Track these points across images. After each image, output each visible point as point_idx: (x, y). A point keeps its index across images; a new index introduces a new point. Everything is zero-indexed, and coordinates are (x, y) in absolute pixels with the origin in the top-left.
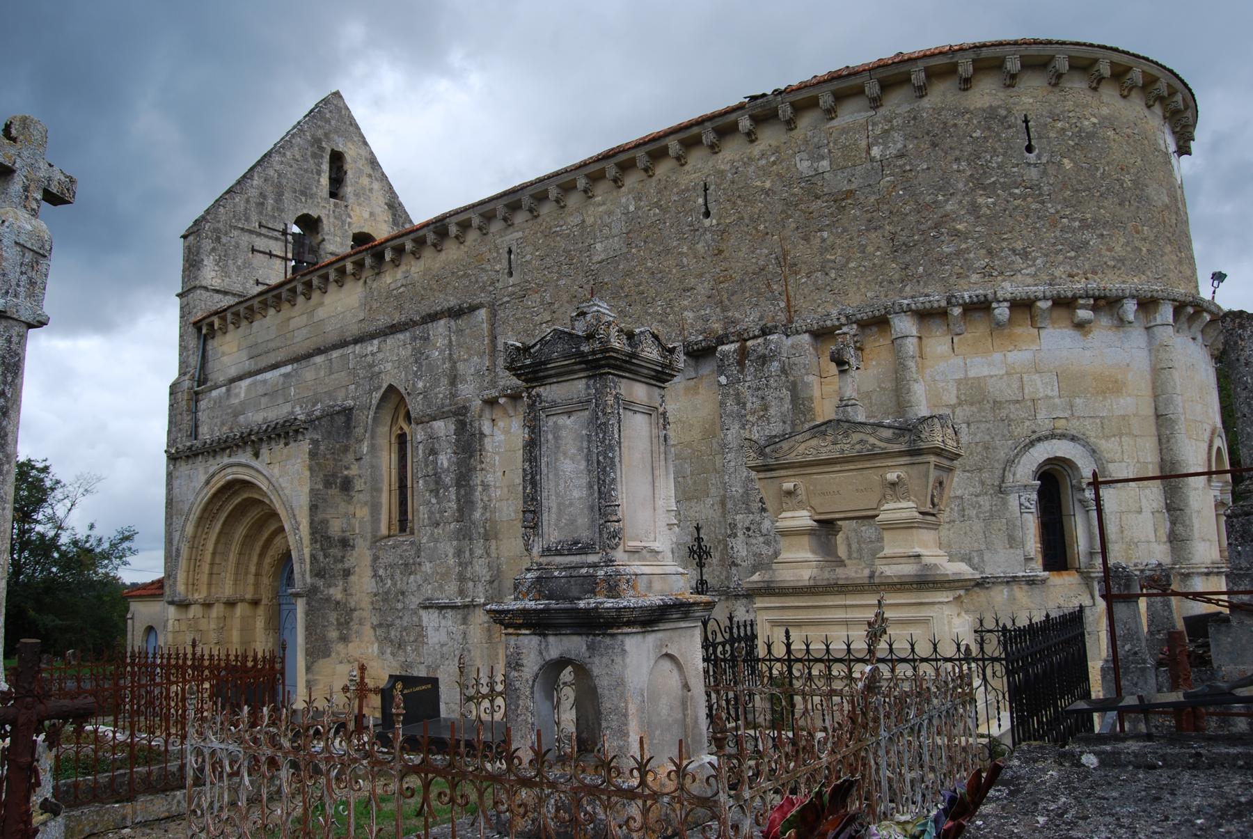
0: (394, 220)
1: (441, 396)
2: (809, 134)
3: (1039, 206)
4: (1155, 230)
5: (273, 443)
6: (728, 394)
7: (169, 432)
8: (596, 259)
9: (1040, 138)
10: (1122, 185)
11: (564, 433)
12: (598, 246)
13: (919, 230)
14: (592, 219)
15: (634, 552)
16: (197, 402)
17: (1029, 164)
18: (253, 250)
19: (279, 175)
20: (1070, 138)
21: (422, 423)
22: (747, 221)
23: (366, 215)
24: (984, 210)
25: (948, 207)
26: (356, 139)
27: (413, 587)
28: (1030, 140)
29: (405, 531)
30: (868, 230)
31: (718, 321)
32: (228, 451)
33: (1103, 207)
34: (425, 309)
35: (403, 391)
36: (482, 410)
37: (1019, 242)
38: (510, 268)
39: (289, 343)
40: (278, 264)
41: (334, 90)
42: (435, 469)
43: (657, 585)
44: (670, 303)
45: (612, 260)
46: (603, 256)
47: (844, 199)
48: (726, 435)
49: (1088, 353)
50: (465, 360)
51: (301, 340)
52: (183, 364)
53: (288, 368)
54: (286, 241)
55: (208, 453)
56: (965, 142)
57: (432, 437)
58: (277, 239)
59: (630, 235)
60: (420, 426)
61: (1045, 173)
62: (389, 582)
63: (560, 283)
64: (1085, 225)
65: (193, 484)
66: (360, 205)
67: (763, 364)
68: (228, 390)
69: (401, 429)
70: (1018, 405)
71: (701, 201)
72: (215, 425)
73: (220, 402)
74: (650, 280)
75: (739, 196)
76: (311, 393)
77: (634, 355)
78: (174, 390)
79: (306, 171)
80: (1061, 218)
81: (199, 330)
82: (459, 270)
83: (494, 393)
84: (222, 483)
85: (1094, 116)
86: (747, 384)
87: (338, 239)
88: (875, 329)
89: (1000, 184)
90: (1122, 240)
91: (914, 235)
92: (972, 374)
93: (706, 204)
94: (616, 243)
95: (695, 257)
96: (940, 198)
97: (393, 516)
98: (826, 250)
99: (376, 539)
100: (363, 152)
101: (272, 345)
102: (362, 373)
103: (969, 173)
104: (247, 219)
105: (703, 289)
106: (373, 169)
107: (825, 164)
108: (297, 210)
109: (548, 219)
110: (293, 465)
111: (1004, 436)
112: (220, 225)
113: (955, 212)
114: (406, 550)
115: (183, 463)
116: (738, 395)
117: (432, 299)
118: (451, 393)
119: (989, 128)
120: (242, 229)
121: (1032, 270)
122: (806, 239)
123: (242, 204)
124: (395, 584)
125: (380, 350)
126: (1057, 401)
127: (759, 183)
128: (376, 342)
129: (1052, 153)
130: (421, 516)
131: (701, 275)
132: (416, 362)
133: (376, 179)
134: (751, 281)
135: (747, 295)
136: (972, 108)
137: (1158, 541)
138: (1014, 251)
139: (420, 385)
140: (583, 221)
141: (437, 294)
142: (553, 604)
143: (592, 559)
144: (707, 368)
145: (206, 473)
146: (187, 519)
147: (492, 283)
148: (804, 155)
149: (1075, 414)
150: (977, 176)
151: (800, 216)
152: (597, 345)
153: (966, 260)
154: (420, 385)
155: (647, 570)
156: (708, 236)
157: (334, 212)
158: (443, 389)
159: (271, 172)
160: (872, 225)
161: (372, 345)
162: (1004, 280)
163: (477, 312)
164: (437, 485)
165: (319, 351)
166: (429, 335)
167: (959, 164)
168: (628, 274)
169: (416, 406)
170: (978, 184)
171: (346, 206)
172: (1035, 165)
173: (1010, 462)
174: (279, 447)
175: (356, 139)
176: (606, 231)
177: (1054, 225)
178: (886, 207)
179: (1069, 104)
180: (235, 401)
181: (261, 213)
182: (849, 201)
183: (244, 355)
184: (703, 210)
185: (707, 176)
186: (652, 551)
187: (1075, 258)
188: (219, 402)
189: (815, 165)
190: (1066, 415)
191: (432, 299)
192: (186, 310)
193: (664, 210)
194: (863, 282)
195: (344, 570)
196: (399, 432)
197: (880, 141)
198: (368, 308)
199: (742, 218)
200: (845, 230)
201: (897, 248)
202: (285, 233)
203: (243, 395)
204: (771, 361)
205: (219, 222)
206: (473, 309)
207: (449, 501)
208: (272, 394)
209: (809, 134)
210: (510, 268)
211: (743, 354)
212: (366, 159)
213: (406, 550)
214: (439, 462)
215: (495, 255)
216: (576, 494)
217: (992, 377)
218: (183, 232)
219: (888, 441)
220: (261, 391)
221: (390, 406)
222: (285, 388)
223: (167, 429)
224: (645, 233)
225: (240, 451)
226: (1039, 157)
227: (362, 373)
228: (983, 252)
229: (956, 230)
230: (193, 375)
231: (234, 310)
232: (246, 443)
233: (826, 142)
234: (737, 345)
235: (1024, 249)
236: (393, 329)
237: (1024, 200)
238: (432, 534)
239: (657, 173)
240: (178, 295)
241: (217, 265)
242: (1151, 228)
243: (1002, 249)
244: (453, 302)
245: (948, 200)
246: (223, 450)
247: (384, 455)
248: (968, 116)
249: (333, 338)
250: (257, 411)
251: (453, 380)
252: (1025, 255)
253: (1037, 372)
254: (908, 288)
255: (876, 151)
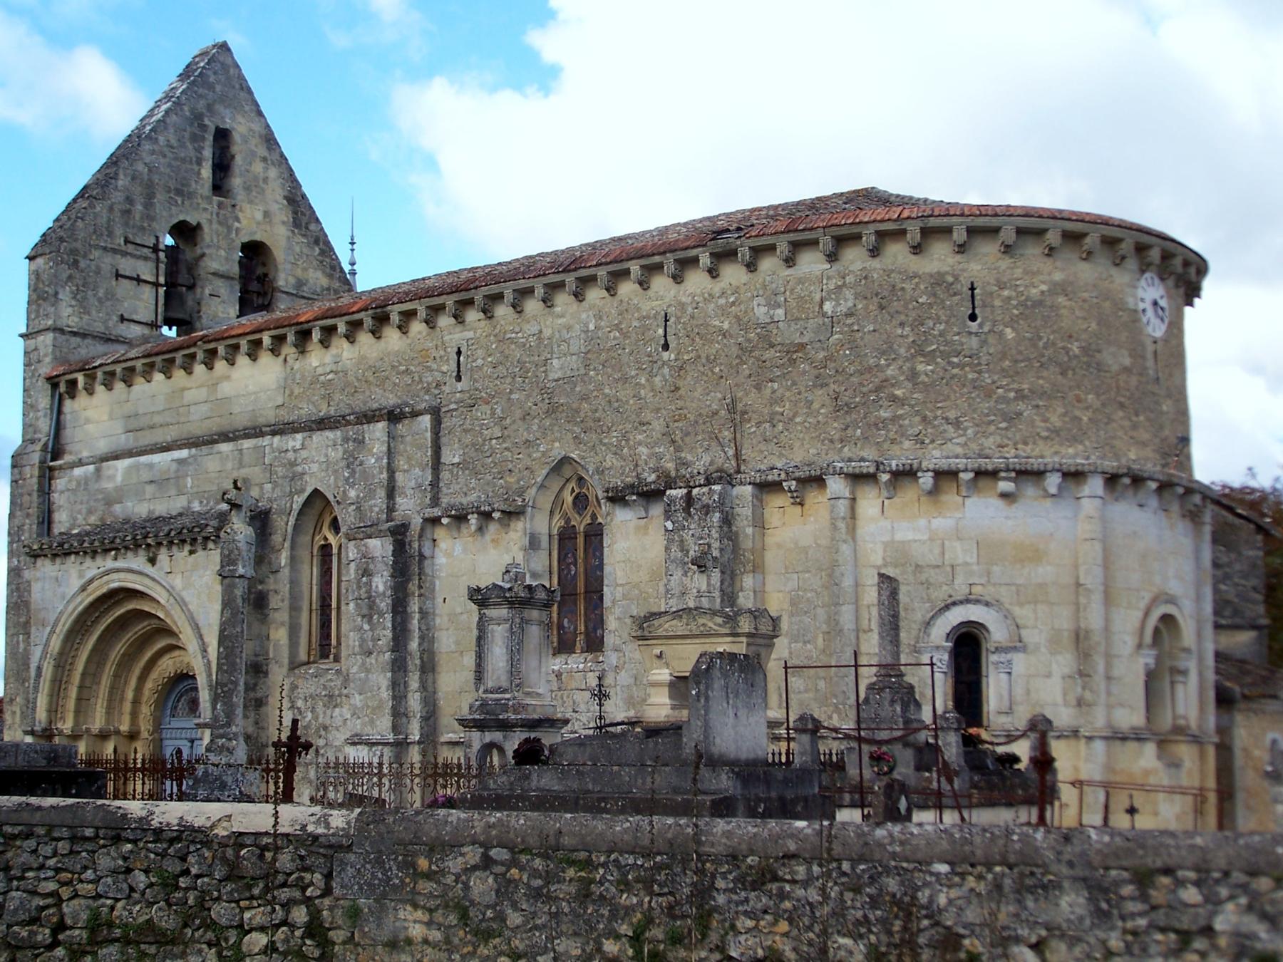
0: (294, 221)
1: (377, 509)
2: (768, 278)
3: (976, 375)
4: (1103, 397)
5: (175, 548)
6: (673, 540)
7: (12, 516)
8: (552, 376)
9: (984, 306)
10: (1067, 353)
11: (496, 634)
12: (555, 362)
13: (861, 392)
14: (550, 331)
15: (528, 694)
16: (50, 479)
17: (970, 333)
18: (118, 276)
19: (150, 170)
20: (1015, 307)
21: (355, 539)
22: (704, 361)
23: (259, 216)
24: (923, 378)
25: (889, 372)
26: (247, 108)
27: (338, 721)
28: (974, 308)
29: (327, 657)
30: (814, 386)
31: (671, 460)
32: (113, 553)
33: (1042, 378)
34: (360, 403)
35: (331, 498)
36: (422, 529)
37: (953, 412)
38: (459, 371)
39: (182, 419)
40: (148, 292)
41: (220, 40)
42: (369, 592)
43: (539, 710)
44: (625, 436)
45: (569, 380)
46: (559, 375)
47: (796, 352)
48: (669, 581)
49: (1010, 523)
50: (405, 471)
51: (199, 420)
52: (28, 426)
53: (184, 453)
54: (158, 260)
55: (85, 553)
56: (910, 306)
57: (366, 556)
58: (146, 258)
59: (589, 356)
60: (353, 543)
61: (984, 343)
62: (310, 715)
63: (513, 396)
64: (1020, 396)
65: (62, 589)
66: (251, 202)
67: (707, 514)
68: (98, 470)
69: (326, 539)
70: (937, 570)
71: (661, 331)
72: (80, 512)
73: (86, 484)
74: (606, 408)
75: (698, 333)
76: (215, 488)
77: (532, 598)
78: (17, 461)
79: (183, 160)
80: (998, 388)
81: (55, 386)
82: (401, 364)
83: (437, 512)
84: (104, 590)
85: (1043, 282)
86: (691, 532)
87: (223, 253)
88: (814, 485)
89: (941, 352)
90: (1061, 410)
91: (856, 397)
92: (899, 536)
93: (665, 336)
94: (574, 362)
95: (652, 390)
96: (883, 362)
97: (314, 640)
98: (776, 402)
99: (294, 666)
100: (257, 127)
101: (157, 419)
102: (280, 471)
103: (911, 339)
104: (110, 234)
105: (658, 425)
106: (269, 149)
107: (780, 313)
108: (171, 216)
109: (503, 322)
110: (201, 577)
111: (922, 598)
112: (78, 245)
113: (894, 378)
114: (331, 680)
115: (47, 562)
116: (682, 541)
117: (368, 393)
118: (388, 507)
119: (935, 295)
120: (105, 249)
121: (962, 440)
122: (758, 387)
123: (105, 214)
124: (316, 718)
125: (303, 447)
126: (975, 568)
127: (717, 323)
128: (299, 436)
129: (994, 322)
130: (351, 643)
131: (658, 410)
132: (348, 467)
133: (273, 164)
134: (704, 423)
135: (700, 438)
136: (921, 273)
137: (1066, 704)
138: (947, 419)
139: (352, 494)
140: (541, 332)
141: (373, 388)
142: (488, 717)
143: (507, 696)
144: (657, 510)
145: (81, 576)
146: (52, 632)
147: (438, 385)
148: (761, 300)
149: (992, 581)
150: (919, 343)
151: (753, 363)
152: (513, 595)
153: (901, 426)
154: (352, 494)
155: (533, 703)
156: (666, 370)
157: (218, 214)
158: (379, 500)
159: (140, 167)
160: (820, 382)
161: (294, 439)
162: (934, 448)
163: (420, 418)
164: (369, 610)
165: (225, 437)
166: (364, 438)
167: (903, 328)
168: (585, 398)
169: (347, 517)
170: (920, 350)
171: (234, 206)
172: (976, 334)
173: (928, 624)
174: (181, 554)
175: (247, 108)
176: (564, 347)
177: (989, 395)
178: (833, 365)
179: (1018, 272)
180: (108, 485)
181: (126, 224)
182: (800, 355)
183: (118, 427)
184: (662, 342)
185: (669, 306)
186: (537, 694)
187: (1006, 429)
188: (85, 482)
189: (772, 312)
190: (983, 581)
191: (368, 393)
192: (34, 356)
193: (625, 335)
194: (807, 438)
195: (256, 700)
196: (323, 542)
197: (833, 296)
198: (287, 392)
199: (699, 357)
200: (794, 383)
201: (840, 407)
202: (155, 249)
203: (119, 478)
204: (714, 512)
205: (76, 240)
206: (415, 414)
207: (384, 629)
208: (160, 482)
209: (768, 278)
210: (459, 371)
211: (689, 500)
212: (260, 136)
213: (331, 680)
214: (374, 585)
215: (442, 353)
216: (501, 664)
217: (915, 541)
218: (27, 252)
219: (720, 625)
220: (146, 476)
221: (313, 513)
222: (179, 477)
223: (8, 512)
224: (603, 356)
225: (130, 554)
226: (981, 326)
227: (280, 471)
228: (917, 419)
229: (894, 395)
230: (46, 445)
231: (108, 369)
232: (138, 546)
233: (782, 289)
234: (685, 491)
235: (956, 418)
236: (322, 424)
237: (962, 369)
238: (363, 664)
239: (619, 293)
240: (21, 336)
241: (74, 298)
242: (1098, 395)
243: (936, 418)
244: (391, 400)
245: (888, 365)
246: (107, 551)
247: (305, 568)
248: (917, 280)
249: (241, 421)
250: (140, 501)
251: (391, 492)
252: (957, 424)
253: (959, 539)
254: (846, 449)
255: (828, 307)
